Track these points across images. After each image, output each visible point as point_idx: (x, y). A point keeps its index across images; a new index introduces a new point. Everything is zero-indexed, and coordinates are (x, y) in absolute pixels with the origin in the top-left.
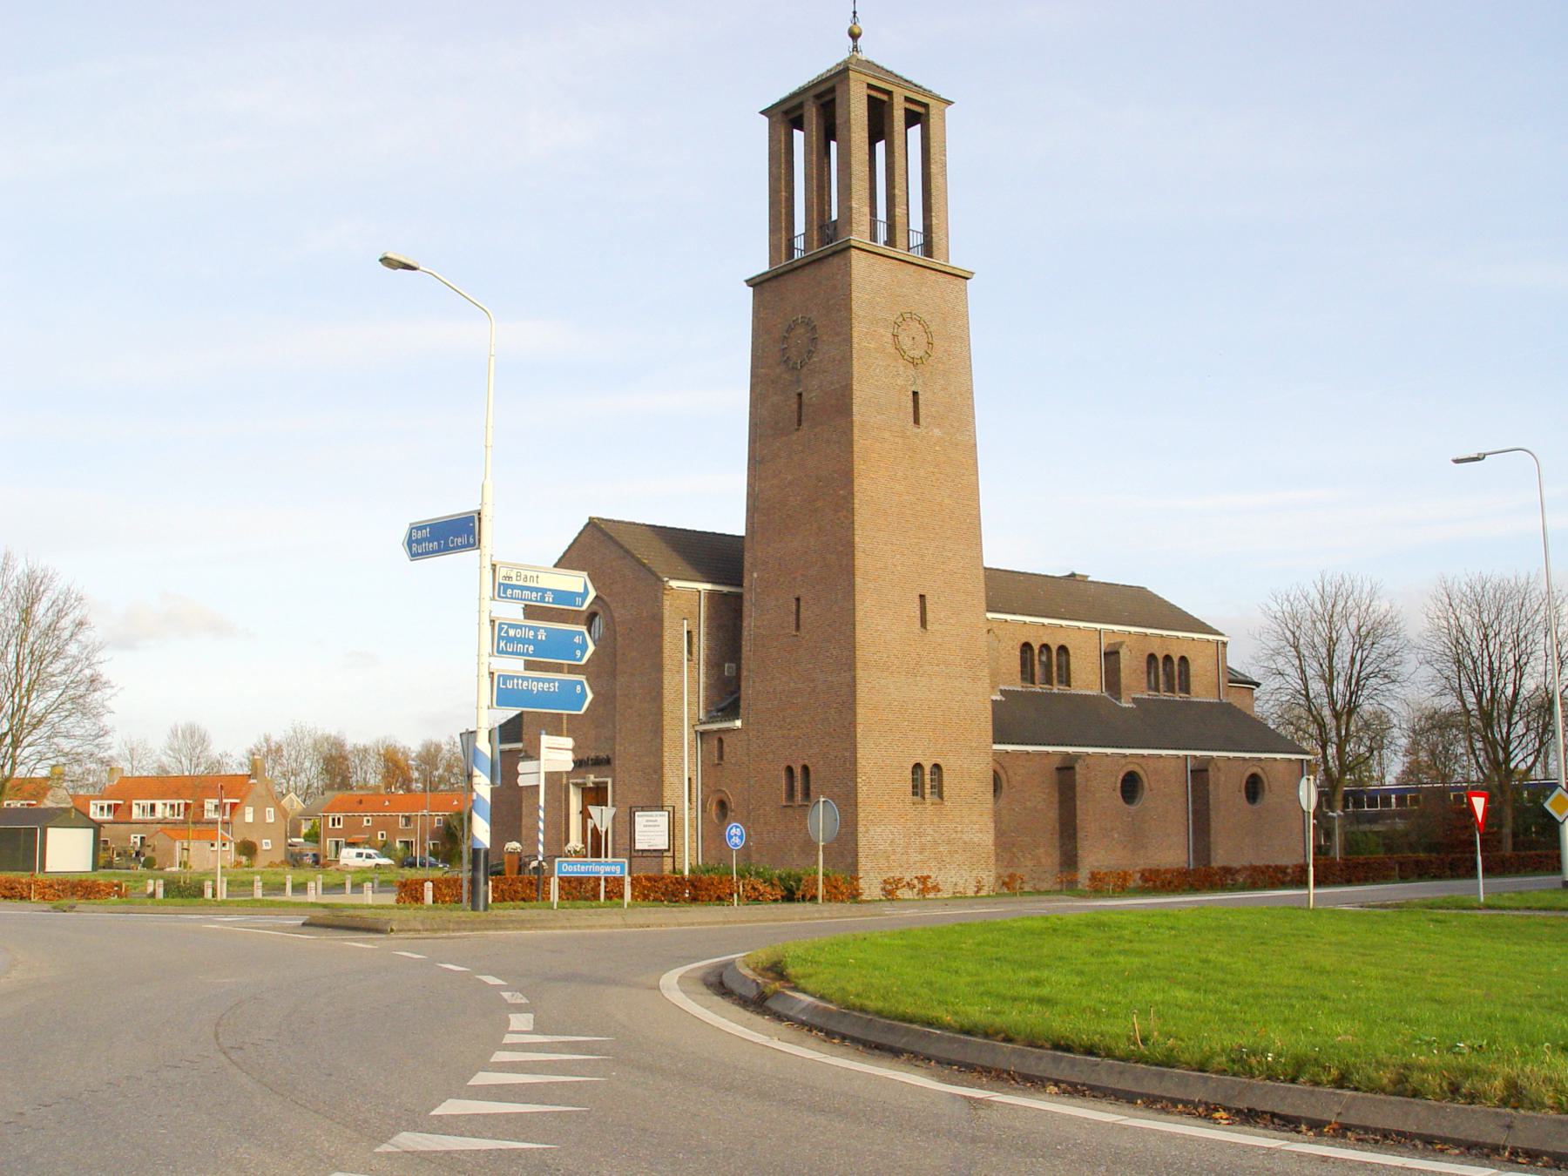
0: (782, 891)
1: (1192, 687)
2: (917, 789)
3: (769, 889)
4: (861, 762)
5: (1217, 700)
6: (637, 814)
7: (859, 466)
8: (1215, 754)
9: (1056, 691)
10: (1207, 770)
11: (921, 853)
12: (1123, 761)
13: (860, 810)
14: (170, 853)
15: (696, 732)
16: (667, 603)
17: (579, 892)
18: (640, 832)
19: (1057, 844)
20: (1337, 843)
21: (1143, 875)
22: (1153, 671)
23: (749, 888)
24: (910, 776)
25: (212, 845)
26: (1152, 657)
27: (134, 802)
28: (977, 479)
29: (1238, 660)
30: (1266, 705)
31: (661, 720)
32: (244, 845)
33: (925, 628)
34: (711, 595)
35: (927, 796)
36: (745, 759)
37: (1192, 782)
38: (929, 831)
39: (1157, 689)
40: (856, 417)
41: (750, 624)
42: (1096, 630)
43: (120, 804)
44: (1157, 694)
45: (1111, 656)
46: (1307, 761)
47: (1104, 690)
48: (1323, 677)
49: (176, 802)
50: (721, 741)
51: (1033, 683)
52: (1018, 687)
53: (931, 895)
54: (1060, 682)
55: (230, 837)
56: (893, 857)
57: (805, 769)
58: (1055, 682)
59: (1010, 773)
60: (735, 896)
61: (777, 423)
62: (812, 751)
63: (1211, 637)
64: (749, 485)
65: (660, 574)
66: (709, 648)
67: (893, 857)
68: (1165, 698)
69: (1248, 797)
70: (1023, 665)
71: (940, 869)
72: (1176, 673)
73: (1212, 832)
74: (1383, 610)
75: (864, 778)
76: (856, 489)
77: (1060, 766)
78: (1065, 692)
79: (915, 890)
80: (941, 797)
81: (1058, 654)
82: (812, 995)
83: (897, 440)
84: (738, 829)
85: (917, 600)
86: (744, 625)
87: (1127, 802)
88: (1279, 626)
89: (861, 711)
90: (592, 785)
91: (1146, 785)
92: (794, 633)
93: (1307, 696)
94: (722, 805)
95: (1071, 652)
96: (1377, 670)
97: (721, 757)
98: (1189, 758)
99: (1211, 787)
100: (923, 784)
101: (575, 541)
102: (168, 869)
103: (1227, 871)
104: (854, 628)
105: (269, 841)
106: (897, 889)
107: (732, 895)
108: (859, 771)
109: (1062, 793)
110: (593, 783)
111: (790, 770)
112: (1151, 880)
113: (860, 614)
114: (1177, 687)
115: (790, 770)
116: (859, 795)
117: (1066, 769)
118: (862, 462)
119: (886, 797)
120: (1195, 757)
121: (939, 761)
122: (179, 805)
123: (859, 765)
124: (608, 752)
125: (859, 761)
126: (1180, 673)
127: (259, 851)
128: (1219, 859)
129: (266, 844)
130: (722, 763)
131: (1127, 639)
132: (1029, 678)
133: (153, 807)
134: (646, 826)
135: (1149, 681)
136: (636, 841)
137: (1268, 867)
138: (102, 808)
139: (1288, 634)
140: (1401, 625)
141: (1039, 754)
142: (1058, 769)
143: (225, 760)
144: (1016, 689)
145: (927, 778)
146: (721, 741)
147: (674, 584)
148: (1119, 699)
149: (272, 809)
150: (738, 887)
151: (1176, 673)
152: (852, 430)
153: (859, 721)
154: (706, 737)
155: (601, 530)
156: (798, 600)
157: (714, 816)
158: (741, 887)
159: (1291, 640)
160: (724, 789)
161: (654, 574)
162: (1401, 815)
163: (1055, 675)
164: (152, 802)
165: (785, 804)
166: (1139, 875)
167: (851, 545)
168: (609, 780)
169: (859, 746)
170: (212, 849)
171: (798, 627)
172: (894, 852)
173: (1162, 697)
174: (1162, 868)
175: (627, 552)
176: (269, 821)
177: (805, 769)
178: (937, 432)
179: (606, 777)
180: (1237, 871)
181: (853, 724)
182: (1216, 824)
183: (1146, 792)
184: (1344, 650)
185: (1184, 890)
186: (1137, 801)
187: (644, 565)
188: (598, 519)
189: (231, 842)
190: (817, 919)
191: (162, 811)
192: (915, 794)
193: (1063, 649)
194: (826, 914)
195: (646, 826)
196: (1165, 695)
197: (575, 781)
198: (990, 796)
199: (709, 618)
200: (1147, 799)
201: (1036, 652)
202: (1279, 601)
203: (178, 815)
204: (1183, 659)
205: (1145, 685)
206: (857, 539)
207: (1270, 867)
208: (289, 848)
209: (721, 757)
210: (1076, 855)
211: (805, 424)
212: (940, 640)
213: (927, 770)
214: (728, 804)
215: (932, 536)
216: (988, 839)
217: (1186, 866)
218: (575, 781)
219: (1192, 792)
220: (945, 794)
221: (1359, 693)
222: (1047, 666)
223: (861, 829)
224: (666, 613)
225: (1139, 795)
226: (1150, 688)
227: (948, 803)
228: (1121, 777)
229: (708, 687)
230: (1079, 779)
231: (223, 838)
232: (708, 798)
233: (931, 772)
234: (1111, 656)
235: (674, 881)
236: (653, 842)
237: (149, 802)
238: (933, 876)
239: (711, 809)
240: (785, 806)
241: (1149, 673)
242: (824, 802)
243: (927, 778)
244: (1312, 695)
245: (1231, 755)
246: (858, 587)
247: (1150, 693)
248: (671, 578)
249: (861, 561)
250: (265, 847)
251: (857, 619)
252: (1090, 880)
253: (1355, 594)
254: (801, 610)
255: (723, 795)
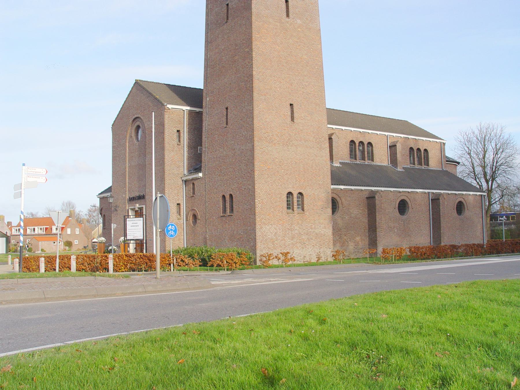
0: (200, 262)
1: (430, 163)
2: (290, 206)
3: (191, 261)
4: (258, 191)
5: (442, 170)
6: (128, 219)
7: (255, 35)
8: (442, 192)
9: (367, 163)
10: (439, 199)
11: (292, 239)
12: (399, 195)
13: (257, 217)
14: (38, 246)
15: (183, 180)
16: (166, 116)
17: (94, 263)
18: (129, 232)
19: (367, 235)
20: (29, 304)
21: (410, 250)
22: (412, 155)
23: (179, 260)
24: (286, 199)
25: (54, 243)
26: (411, 149)
27: (28, 227)
28: (321, 47)
29: (450, 154)
30: (461, 172)
31: (164, 175)
32: (67, 242)
33: (293, 121)
34: (190, 112)
35: (295, 209)
36: (204, 193)
37: (432, 205)
38: (296, 228)
39: (414, 164)
40: (254, 10)
41: (206, 124)
42: (385, 135)
43: (48, 228)
44: (414, 166)
45: (393, 147)
46: (484, 196)
47: (389, 164)
48: (481, 166)
49: (42, 227)
50: (193, 184)
51: (356, 159)
52: (348, 161)
53: (290, 263)
54: (369, 159)
55: (61, 239)
56: (276, 242)
57: (231, 196)
58: (366, 159)
59: (343, 200)
60: (172, 265)
61: (217, 21)
62: (234, 187)
63: (438, 141)
64: (205, 55)
65: (163, 102)
66: (189, 139)
67: (276, 242)
68: (418, 168)
69: (458, 213)
70: (351, 151)
71: (303, 248)
72: (423, 157)
73: (442, 228)
74: (505, 138)
75: (259, 199)
76: (253, 47)
77: (368, 196)
78: (371, 164)
79: (280, 260)
80: (303, 210)
81: (367, 146)
82: (334, 274)
83: (277, 24)
84: (173, 227)
85: (289, 106)
86: (203, 125)
87: (401, 214)
88: (462, 145)
89: (257, 164)
90: (137, 209)
91: (410, 205)
92: (225, 126)
93: (475, 174)
94: (195, 217)
95: (374, 146)
96: (504, 162)
97: (194, 193)
98: (430, 193)
99: (441, 207)
100: (293, 203)
101: (130, 92)
102: (36, 252)
103: (454, 247)
104: (253, 120)
105: (77, 241)
106: (269, 260)
107: (170, 264)
108: (256, 195)
109: (369, 209)
110: (138, 208)
111: (224, 197)
112: (415, 253)
113: (256, 112)
114: (423, 163)
115: (224, 197)
116: (257, 209)
117: (371, 198)
118: (257, 33)
119: (272, 210)
120: (433, 193)
121: (301, 191)
122: (43, 228)
123: (256, 193)
124: (144, 193)
125: (256, 190)
126: (424, 156)
127: (73, 245)
128: (446, 241)
129: (76, 242)
130: (194, 195)
131: (400, 140)
132: (354, 157)
133: (34, 229)
134: (132, 226)
135: (410, 160)
136: (127, 234)
137: (474, 244)
138: (16, 230)
139: (466, 148)
140: (514, 143)
141: (358, 190)
142: (367, 198)
143: (81, 213)
144: (347, 162)
145: (295, 200)
146: (193, 184)
147: (170, 106)
148: (396, 167)
149: (78, 229)
150: (173, 260)
151: (423, 157)
152: (251, 17)
153: (256, 169)
154: (187, 183)
155: (140, 85)
156: (227, 108)
157: (191, 222)
158: (175, 260)
159: (467, 151)
160: (195, 209)
161: (161, 103)
162: (514, 223)
163: (366, 156)
164: (34, 227)
165: (222, 215)
166: (409, 249)
167: (251, 76)
168: (144, 206)
169: (256, 182)
170: (54, 244)
171: (227, 124)
172: (277, 239)
173: (416, 167)
174: (421, 246)
175: (150, 93)
176: (77, 233)
177: (231, 196)
178: (299, 22)
179: (143, 205)
180: (459, 247)
181: (253, 171)
182: (443, 224)
183: (410, 210)
184: (490, 156)
185: (432, 258)
186: (406, 213)
187: (156, 99)
188: (140, 80)
189: (62, 241)
190: (140, 293)
191: (38, 231)
192: (288, 208)
193: (370, 144)
194: (150, 288)
195: (132, 226)
196: (417, 166)
197: (131, 207)
198: (330, 210)
199: (189, 124)
200: (410, 212)
201: (357, 145)
202: (462, 135)
203: (43, 232)
204: (426, 150)
205: (409, 162)
206: (254, 73)
207: (475, 244)
208: (93, 243)
209: (194, 193)
210: (376, 240)
211: (230, 19)
212: (301, 128)
213: (295, 196)
214: (197, 217)
215: (297, 74)
216: (328, 232)
217: (429, 244)
218: (131, 207)
219: (432, 209)
220: (305, 208)
221: (496, 172)
222: (363, 152)
223: (258, 227)
224: (166, 122)
225: (407, 211)
226: (411, 163)
227: (307, 213)
228: (398, 202)
229: (189, 158)
230: (377, 202)
231: (60, 240)
232: (189, 213)
233: (298, 197)
234: (393, 147)
235: (139, 257)
236: (135, 235)
237: (33, 227)
238: (291, 252)
239: (190, 219)
240: (222, 216)
241: (410, 156)
242: (160, 197)
243: (295, 200)
244: (476, 173)
245: (450, 192)
246: (255, 98)
247: (411, 165)
248: (168, 104)
249: (257, 84)
250: (75, 243)
251: (255, 114)
252: (382, 253)
253: (494, 131)
254: (229, 113)
255: (195, 212)
